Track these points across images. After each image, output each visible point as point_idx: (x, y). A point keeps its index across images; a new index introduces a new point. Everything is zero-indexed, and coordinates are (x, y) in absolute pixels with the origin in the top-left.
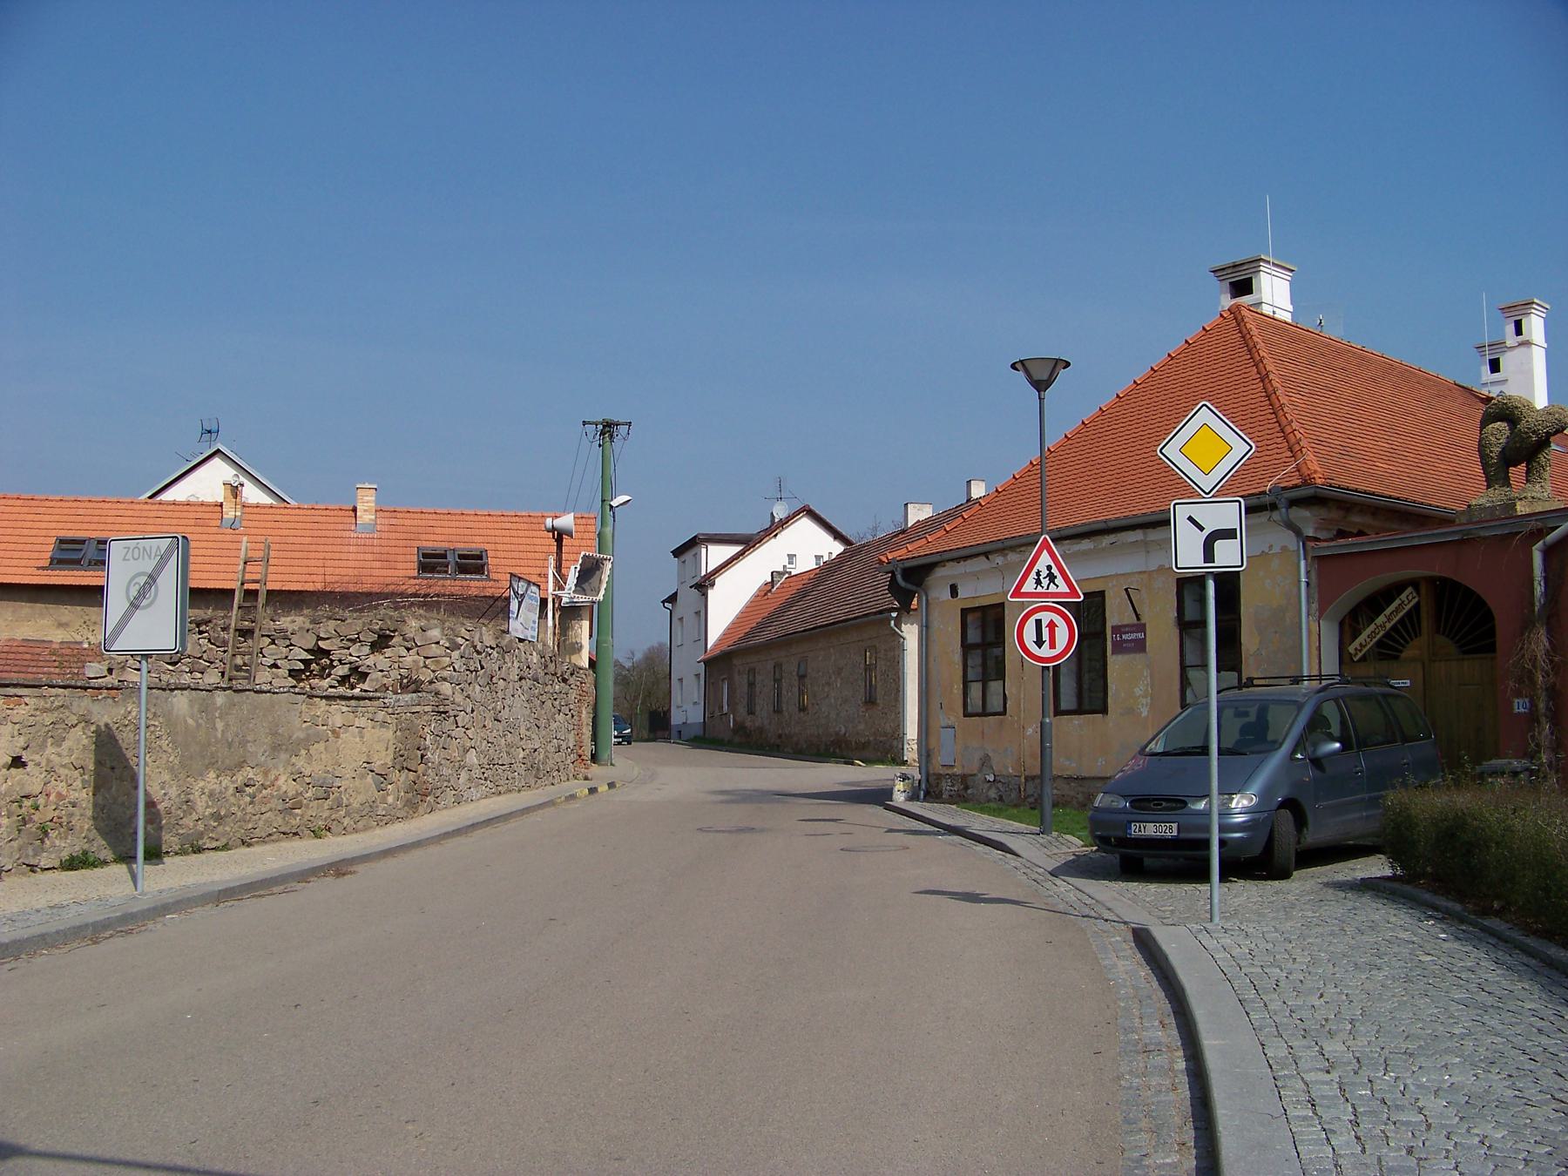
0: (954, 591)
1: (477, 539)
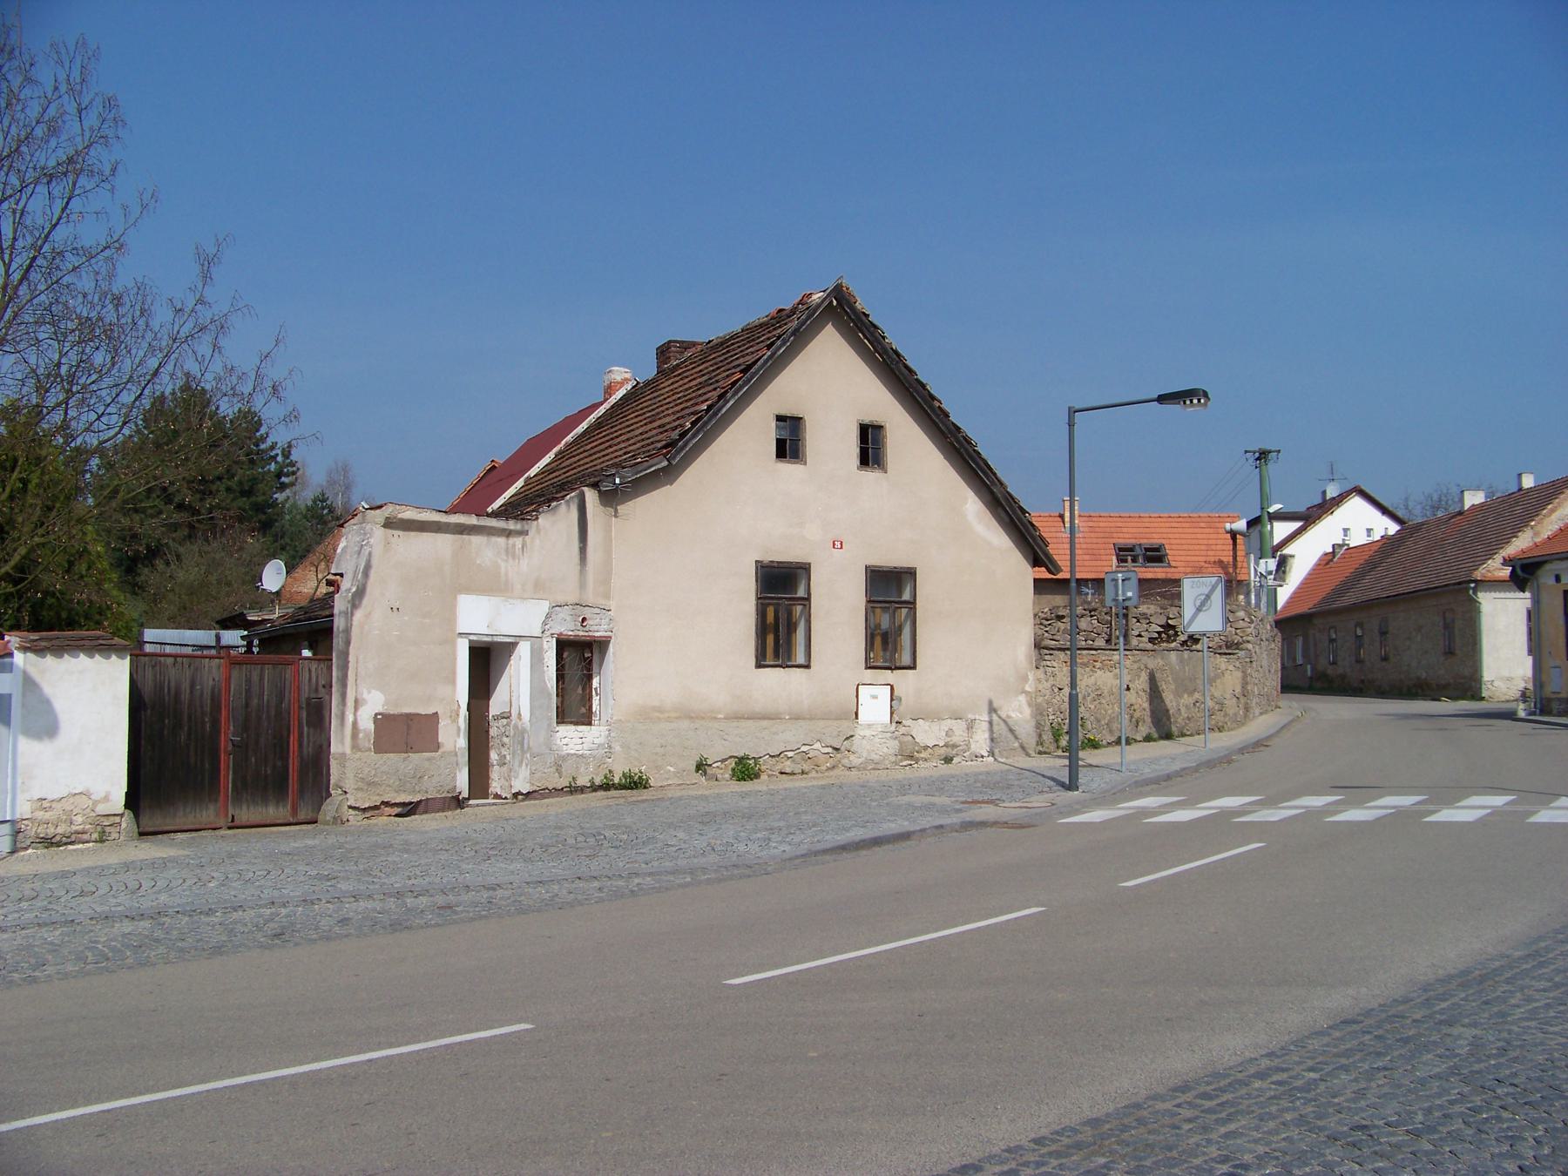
0: (1558, 579)
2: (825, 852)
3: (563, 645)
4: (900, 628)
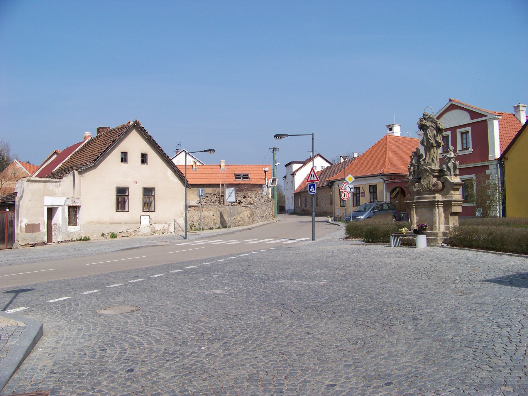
1: (246, 171)
2: (120, 250)
3: (69, 207)
4: (152, 202)
